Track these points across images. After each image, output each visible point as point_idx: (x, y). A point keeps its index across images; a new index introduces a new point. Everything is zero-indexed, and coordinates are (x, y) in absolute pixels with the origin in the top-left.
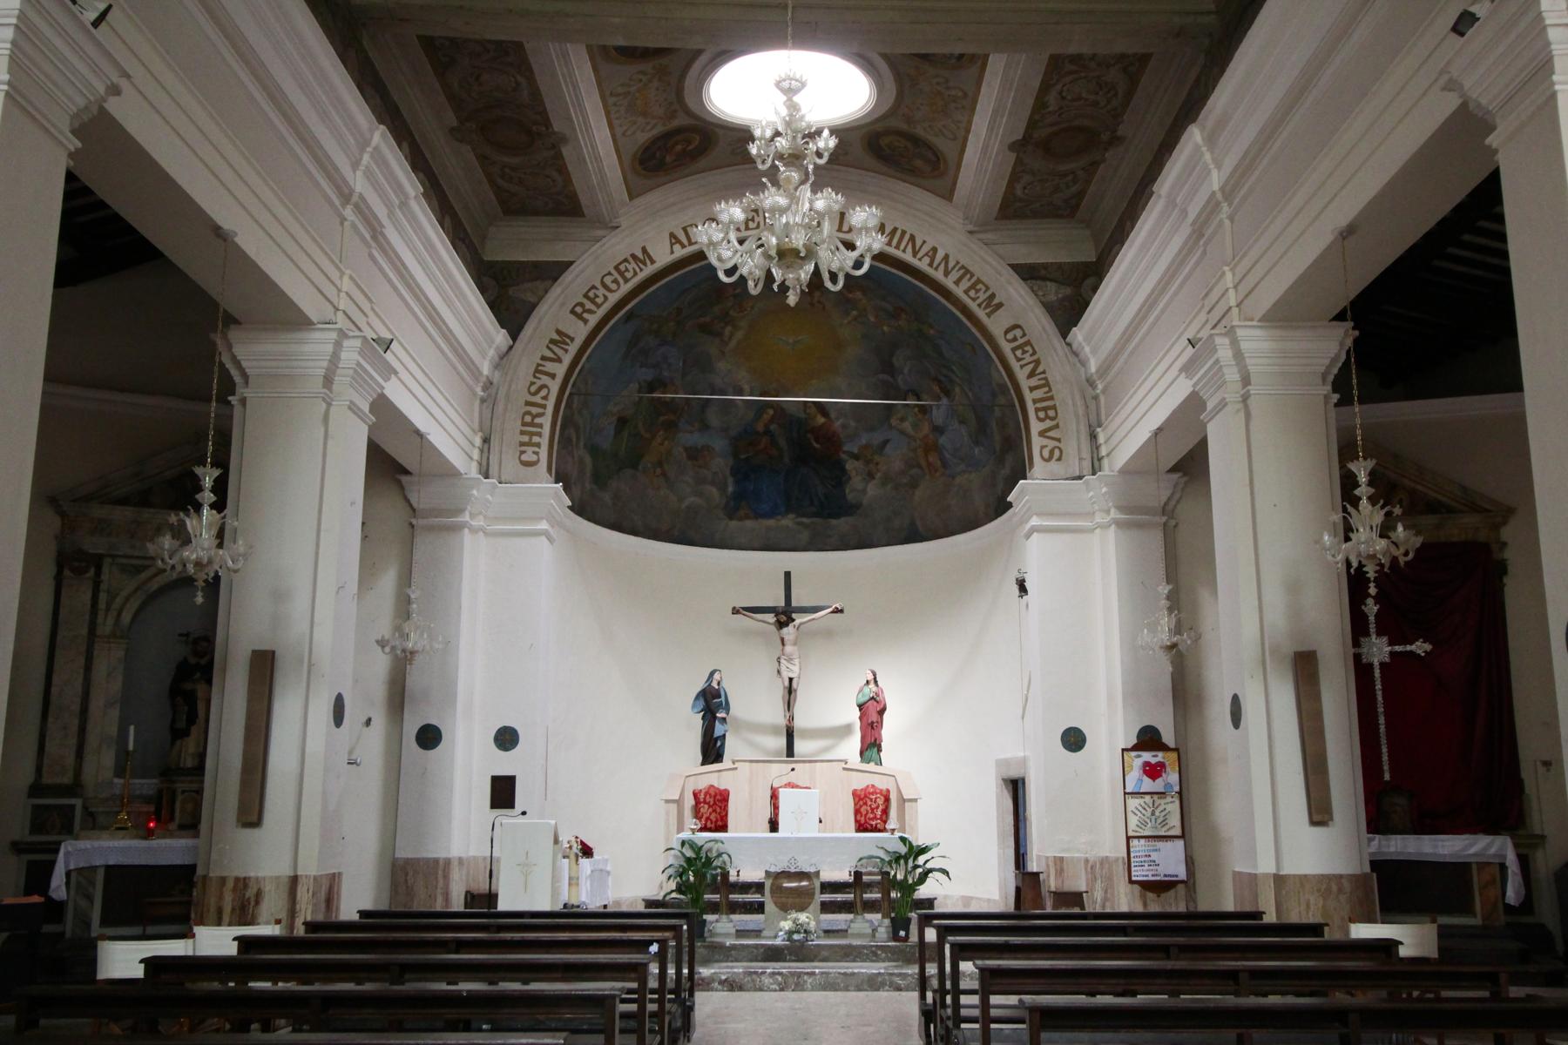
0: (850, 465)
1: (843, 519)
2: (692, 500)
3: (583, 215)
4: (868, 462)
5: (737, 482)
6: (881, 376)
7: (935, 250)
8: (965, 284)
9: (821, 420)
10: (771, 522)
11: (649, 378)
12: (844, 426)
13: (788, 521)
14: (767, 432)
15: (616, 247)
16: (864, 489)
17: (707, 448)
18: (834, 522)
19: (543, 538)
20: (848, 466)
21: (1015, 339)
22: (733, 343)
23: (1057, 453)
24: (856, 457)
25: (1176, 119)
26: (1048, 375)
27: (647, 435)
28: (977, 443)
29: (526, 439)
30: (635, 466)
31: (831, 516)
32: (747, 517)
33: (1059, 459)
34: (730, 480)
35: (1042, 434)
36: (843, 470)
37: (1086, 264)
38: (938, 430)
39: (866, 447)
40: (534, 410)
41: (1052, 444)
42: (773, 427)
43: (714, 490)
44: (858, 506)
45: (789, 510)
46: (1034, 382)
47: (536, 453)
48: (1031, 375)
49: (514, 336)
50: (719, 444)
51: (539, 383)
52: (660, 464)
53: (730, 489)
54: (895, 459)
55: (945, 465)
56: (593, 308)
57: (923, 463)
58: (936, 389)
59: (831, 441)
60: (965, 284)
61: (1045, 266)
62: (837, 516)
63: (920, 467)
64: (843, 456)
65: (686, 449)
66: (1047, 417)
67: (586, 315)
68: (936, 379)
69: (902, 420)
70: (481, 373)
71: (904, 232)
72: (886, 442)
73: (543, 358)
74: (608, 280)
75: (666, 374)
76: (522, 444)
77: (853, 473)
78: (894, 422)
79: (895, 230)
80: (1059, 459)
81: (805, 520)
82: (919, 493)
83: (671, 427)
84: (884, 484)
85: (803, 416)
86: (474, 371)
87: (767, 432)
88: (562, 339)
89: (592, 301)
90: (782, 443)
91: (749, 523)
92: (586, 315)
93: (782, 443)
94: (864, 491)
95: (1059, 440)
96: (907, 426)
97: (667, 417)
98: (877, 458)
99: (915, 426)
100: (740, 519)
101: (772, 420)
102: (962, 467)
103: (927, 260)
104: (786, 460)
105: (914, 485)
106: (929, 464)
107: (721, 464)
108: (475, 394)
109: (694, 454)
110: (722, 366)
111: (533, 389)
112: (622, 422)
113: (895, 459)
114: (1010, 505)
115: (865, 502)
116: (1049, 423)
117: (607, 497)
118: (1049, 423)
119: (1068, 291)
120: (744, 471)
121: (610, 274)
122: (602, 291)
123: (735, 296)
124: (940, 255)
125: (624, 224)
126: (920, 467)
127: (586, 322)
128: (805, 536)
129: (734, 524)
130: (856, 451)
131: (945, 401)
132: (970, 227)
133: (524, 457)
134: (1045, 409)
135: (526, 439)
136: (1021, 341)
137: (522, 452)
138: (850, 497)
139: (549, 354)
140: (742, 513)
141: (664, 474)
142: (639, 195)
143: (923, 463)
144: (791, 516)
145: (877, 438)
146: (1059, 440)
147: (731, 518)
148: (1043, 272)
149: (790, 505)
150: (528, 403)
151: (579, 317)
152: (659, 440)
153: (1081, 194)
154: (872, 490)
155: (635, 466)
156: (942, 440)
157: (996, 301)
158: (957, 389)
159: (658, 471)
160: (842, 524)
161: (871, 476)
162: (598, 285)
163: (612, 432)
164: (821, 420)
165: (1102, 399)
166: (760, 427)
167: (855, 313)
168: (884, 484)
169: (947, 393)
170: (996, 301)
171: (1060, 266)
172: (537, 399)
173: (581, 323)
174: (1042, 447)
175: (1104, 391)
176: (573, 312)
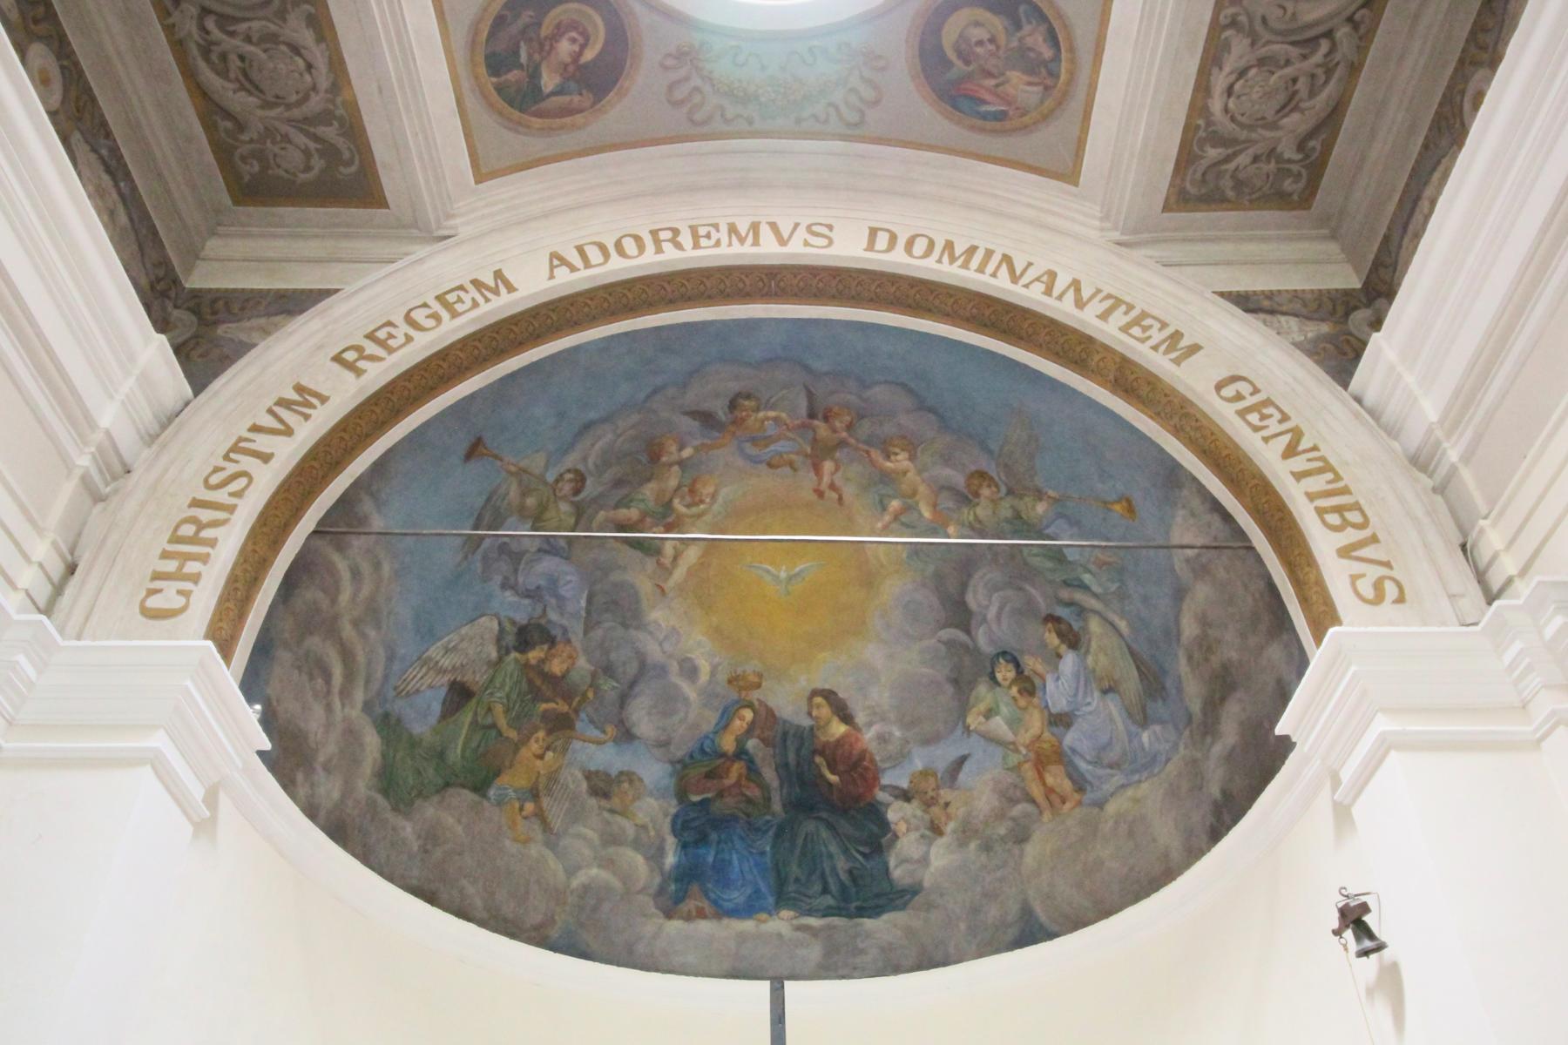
0: (896, 813)
1: (885, 917)
2: (593, 873)
3: (383, 204)
4: (929, 804)
5: (684, 846)
6: (946, 634)
7: (1052, 275)
8: (1119, 318)
9: (839, 729)
10: (747, 925)
11: (521, 618)
12: (882, 739)
13: (781, 923)
14: (741, 753)
15: (442, 267)
16: (920, 853)
17: (629, 776)
18: (868, 923)
19: (147, 772)
20: (891, 815)
21: (1239, 397)
22: (679, 573)
23: (1391, 590)
24: (906, 796)
25: (1415, 171)
26: (1324, 451)
27: (513, 734)
28: (1145, 721)
29: (171, 566)
30: (480, 788)
31: (861, 912)
32: (701, 914)
33: (1401, 599)
34: (671, 842)
35: (1345, 552)
36: (884, 825)
37: (1347, 293)
38: (1061, 721)
39: (926, 773)
40: (206, 515)
41: (1376, 572)
42: (751, 744)
43: (640, 859)
44: (914, 891)
45: (782, 899)
46: (1299, 463)
47: (185, 594)
48: (1290, 451)
49: (196, 393)
50: (654, 772)
51: (232, 468)
52: (535, 794)
53: (671, 859)
54: (979, 791)
55: (1080, 784)
56: (380, 352)
57: (1037, 791)
58: (1053, 640)
59: (858, 768)
60: (1119, 318)
61: (1270, 295)
62: (875, 911)
63: (1033, 801)
64: (882, 796)
65: (589, 776)
66: (1346, 524)
67: (361, 364)
68: (1051, 619)
69: (989, 714)
70: (92, 425)
71: (989, 253)
72: (962, 760)
73: (256, 429)
74: (419, 316)
75: (553, 616)
76: (157, 576)
77: (902, 827)
78: (973, 720)
79: (972, 250)
80: (1401, 599)
81: (813, 921)
82: (1032, 851)
83: (561, 725)
84: (962, 843)
85: (807, 723)
86: (80, 418)
87: (741, 753)
88: (305, 398)
89: (382, 343)
90: (770, 775)
91: (705, 926)
92: (361, 364)
93: (770, 775)
94: (924, 861)
95: (1388, 565)
96: (999, 725)
97: (553, 705)
98: (946, 794)
99: (1014, 723)
100: (688, 918)
101: (749, 732)
102: (1118, 779)
103: (1039, 288)
104: (777, 806)
105: (1021, 836)
106: (1049, 791)
107: (653, 809)
108: (68, 465)
109: (602, 786)
110: (658, 615)
111: (214, 480)
112: (460, 694)
113: (979, 791)
114: (1285, 746)
115: (926, 884)
116: (1351, 536)
117: (408, 829)
118: (1351, 536)
119: (1325, 328)
120: (699, 824)
121: (425, 305)
122: (405, 328)
123: (681, 463)
124: (1061, 283)
125: (464, 232)
126: (1033, 801)
127: (359, 372)
128: (814, 952)
129: (675, 926)
130: (905, 784)
131: (1069, 661)
132: (1116, 235)
133: (153, 602)
134: (1339, 510)
135: (171, 566)
136: (1250, 401)
137: (152, 592)
138: (898, 873)
139: (269, 422)
140: (690, 905)
141: (540, 815)
142: (494, 175)
143: (1037, 791)
144: (785, 913)
145: (942, 756)
146: (1388, 565)
147: (669, 915)
148: (1266, 303)
149: (784, 893)
150: (196, 503)
151: (350, 366)
152: (535, 747)
153: (1336, 113)
154: (941, 857)
155: (480, 788)
156: (1070, 738)
157: (1184, 343)
158: (1095, 625)
159: (529, 807)
160: (882, 927)
161: (936, 830)
162: (399, 319)
163: (437, 708)
164: (839, 729)
165: (1466, 474)
166: (728, 744)
167: (895, 504)
168: (962, 843)
169: (1073, 640)
170: (1184, 343)
171: (1296, 295)
172: (221, 496)
173: (349, 376)
174: (1354, 579)
175: (1466, 458)
176: (338, 359)
